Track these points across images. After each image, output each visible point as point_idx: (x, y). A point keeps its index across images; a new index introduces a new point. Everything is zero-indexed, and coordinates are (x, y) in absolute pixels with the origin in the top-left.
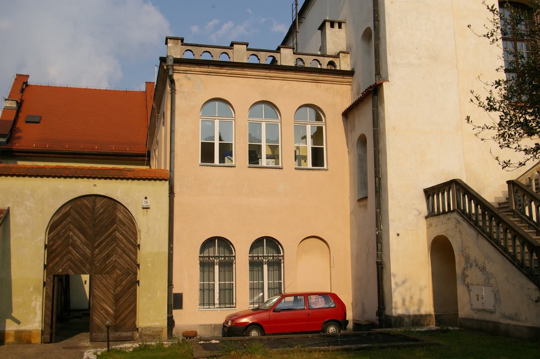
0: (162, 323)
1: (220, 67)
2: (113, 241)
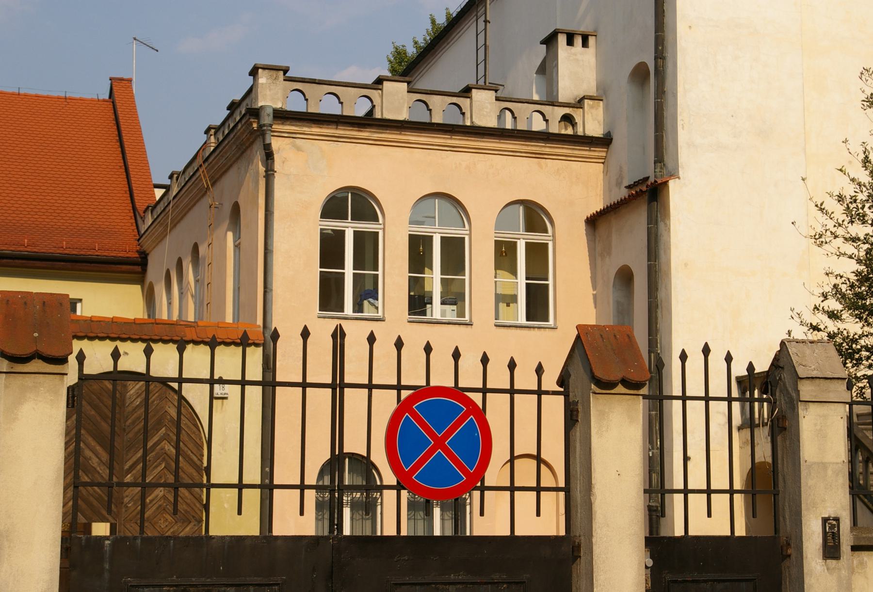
1: (358, 127)
2: (159, 459)
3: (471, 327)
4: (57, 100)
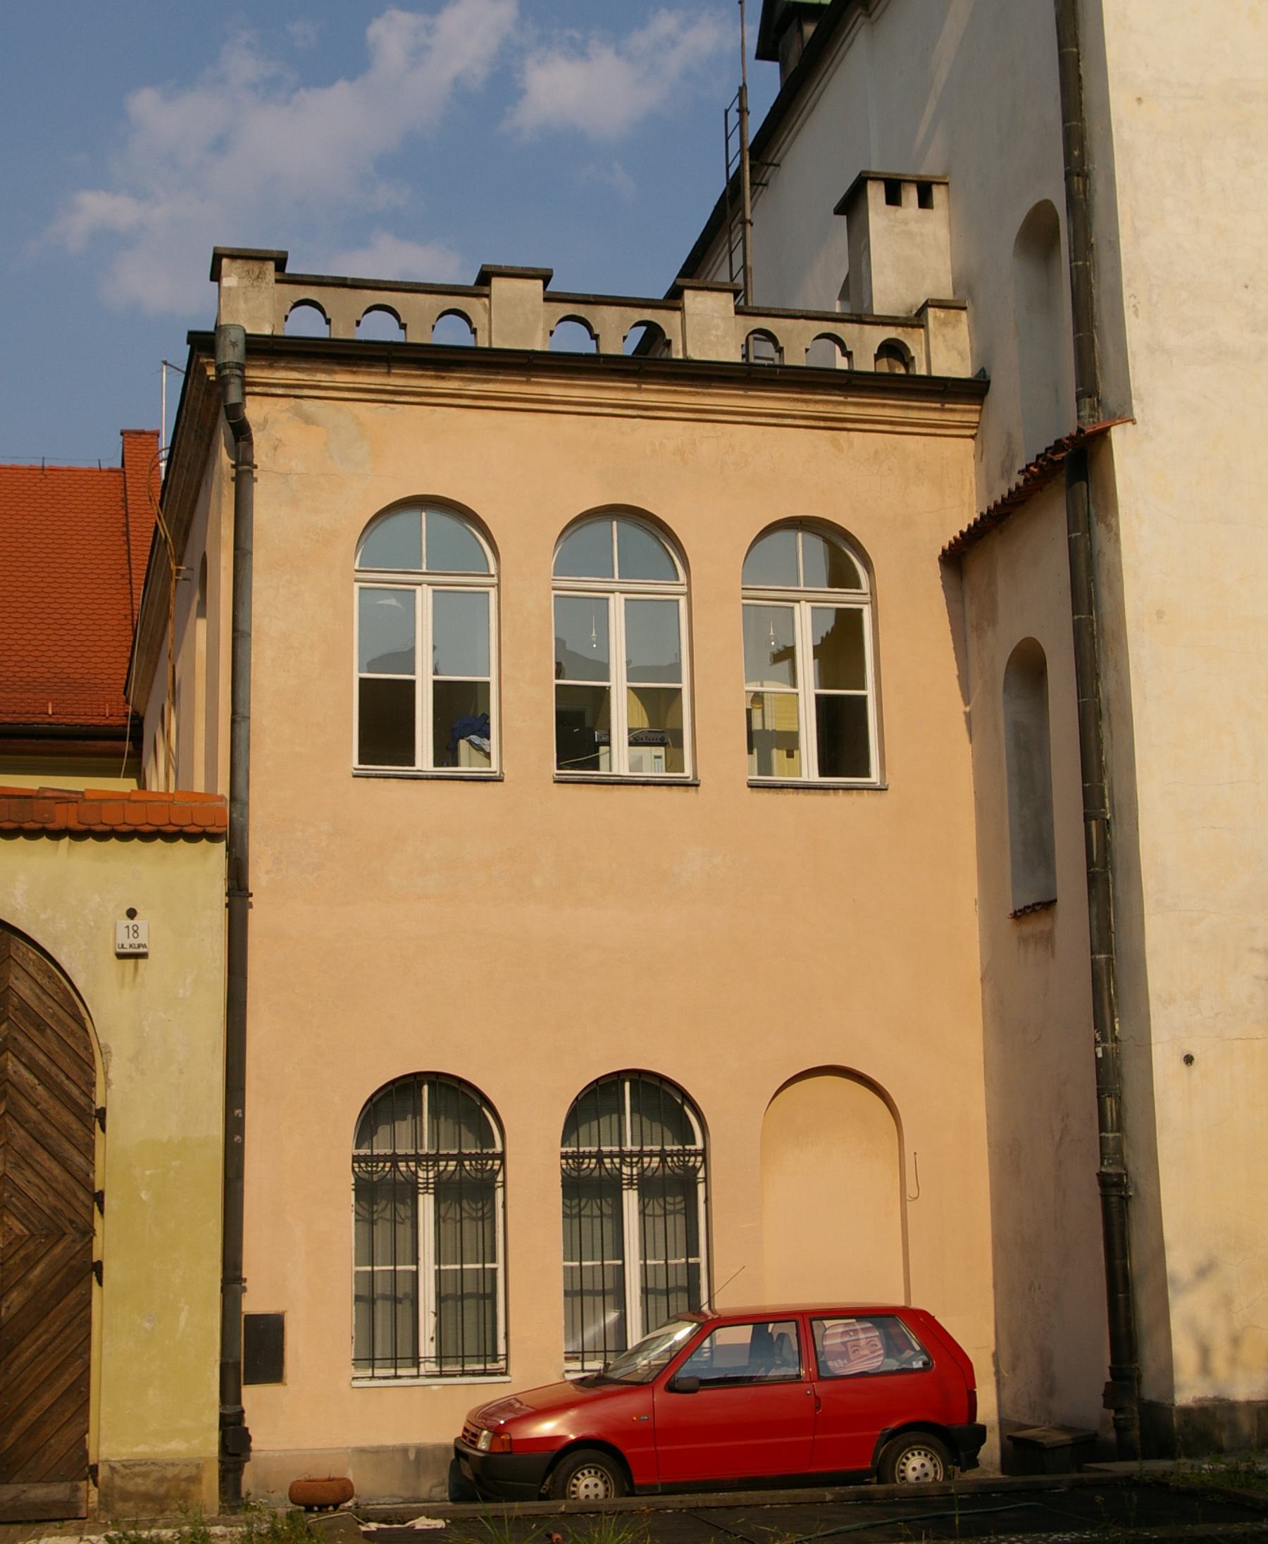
0: (195, 1442)
1: (435, 370)
3: (697, 791)
4: (27, 471)
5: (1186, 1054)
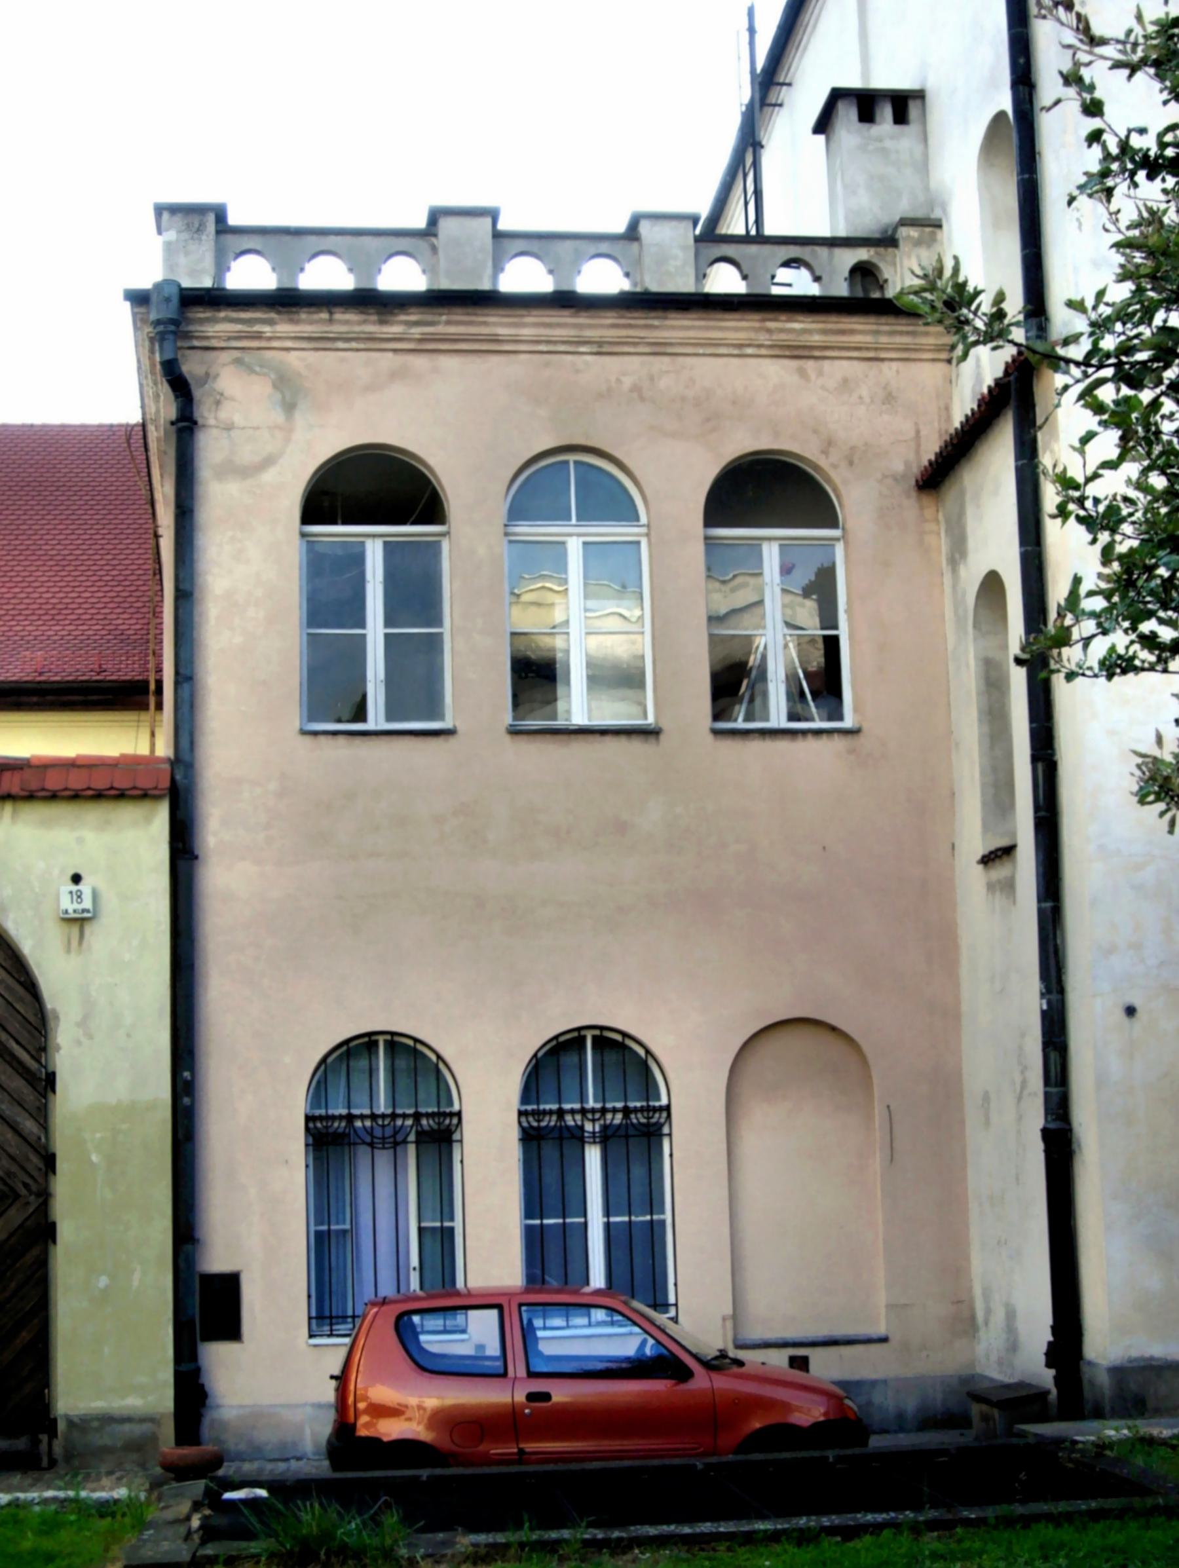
0: (150, 1398)
5: (1127, 1005)
